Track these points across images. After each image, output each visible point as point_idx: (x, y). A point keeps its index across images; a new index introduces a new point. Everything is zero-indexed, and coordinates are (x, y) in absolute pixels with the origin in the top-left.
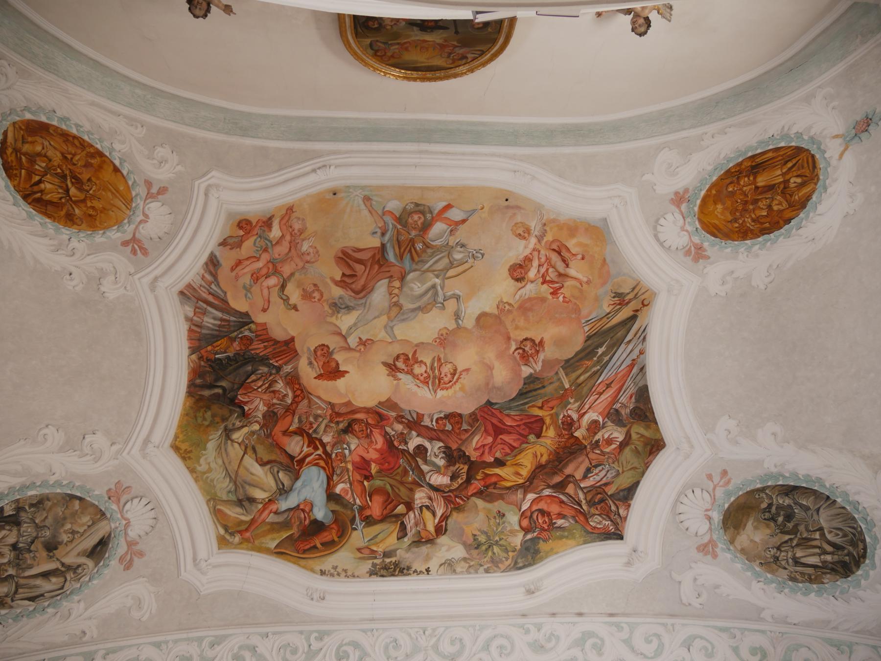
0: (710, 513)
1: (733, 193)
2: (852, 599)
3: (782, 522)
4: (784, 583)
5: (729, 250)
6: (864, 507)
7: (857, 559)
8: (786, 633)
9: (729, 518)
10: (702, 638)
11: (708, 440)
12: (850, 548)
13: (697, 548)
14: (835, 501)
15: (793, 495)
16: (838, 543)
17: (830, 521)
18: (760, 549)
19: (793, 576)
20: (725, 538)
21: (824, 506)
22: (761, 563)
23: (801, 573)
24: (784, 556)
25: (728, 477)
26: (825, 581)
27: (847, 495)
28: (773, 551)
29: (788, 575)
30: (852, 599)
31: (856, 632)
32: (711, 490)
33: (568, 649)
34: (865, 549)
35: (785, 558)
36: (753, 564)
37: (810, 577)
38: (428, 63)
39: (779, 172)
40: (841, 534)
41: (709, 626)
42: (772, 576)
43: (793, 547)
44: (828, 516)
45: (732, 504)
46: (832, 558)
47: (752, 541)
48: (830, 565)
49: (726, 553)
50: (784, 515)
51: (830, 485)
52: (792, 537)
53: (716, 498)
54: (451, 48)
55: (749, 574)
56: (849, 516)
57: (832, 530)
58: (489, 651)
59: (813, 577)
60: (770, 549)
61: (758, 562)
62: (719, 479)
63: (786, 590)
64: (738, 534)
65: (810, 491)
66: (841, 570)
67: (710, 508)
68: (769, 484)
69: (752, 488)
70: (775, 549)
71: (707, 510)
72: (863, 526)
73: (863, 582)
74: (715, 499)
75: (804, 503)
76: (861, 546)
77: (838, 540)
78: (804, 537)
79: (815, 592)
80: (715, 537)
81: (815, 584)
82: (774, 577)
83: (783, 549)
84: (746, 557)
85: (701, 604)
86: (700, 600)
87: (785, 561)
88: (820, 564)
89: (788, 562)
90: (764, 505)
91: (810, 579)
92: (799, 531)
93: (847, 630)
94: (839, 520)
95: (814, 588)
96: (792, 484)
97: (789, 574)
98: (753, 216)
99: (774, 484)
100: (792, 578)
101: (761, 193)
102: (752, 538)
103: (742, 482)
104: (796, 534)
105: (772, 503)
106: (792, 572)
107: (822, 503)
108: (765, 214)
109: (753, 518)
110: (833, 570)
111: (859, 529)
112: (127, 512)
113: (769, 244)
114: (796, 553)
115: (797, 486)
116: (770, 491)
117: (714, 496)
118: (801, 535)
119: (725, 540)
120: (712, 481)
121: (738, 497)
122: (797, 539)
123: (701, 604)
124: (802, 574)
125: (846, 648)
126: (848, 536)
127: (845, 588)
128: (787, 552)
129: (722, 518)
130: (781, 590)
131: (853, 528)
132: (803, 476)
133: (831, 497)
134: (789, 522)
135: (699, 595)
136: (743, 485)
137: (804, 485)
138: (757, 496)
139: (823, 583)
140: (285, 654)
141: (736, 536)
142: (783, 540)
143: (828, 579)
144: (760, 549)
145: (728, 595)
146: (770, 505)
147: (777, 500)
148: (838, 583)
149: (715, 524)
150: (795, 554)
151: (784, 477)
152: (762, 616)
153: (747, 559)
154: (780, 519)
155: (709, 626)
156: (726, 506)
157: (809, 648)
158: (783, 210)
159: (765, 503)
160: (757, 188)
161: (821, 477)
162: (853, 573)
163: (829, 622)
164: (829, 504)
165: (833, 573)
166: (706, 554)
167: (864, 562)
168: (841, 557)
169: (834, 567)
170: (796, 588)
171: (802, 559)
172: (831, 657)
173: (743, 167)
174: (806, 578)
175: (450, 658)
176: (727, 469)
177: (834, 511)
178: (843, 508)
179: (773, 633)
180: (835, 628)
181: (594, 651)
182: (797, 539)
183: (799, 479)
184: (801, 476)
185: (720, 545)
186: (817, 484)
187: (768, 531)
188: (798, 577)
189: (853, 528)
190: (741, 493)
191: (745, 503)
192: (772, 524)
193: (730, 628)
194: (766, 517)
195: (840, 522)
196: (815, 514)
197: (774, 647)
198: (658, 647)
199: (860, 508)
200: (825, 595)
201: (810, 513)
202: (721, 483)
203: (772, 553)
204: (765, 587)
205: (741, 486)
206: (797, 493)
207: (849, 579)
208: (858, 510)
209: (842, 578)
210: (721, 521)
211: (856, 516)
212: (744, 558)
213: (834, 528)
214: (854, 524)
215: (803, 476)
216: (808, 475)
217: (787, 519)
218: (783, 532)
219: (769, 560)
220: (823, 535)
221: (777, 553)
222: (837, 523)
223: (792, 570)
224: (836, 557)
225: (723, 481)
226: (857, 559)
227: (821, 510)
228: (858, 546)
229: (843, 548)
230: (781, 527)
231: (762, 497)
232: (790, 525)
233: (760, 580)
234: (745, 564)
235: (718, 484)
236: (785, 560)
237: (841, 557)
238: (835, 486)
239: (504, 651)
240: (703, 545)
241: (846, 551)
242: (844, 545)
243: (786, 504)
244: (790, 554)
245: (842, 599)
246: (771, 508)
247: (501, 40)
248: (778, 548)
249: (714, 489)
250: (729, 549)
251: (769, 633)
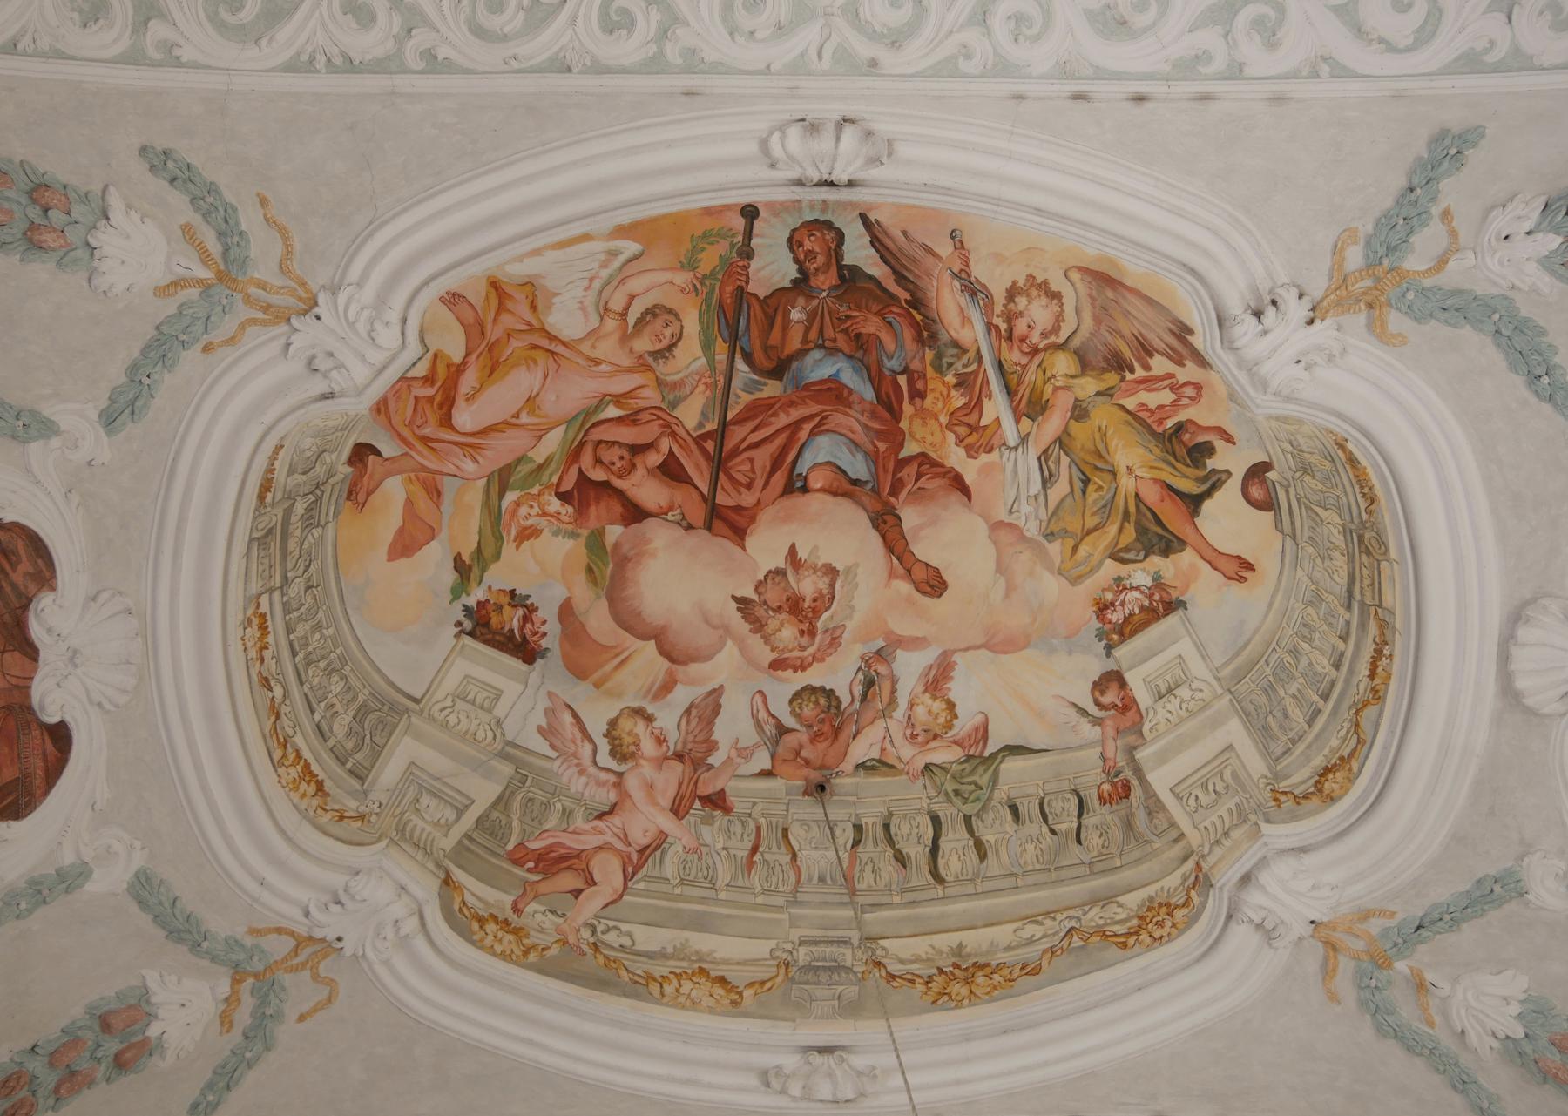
33: (1190, 31)
58: (987, 28)
112: (42, 610)
140: (473, 11)
175: (888, 41)
181: (1257, 38)
198: (1425, 22)
239: (1024, 29)
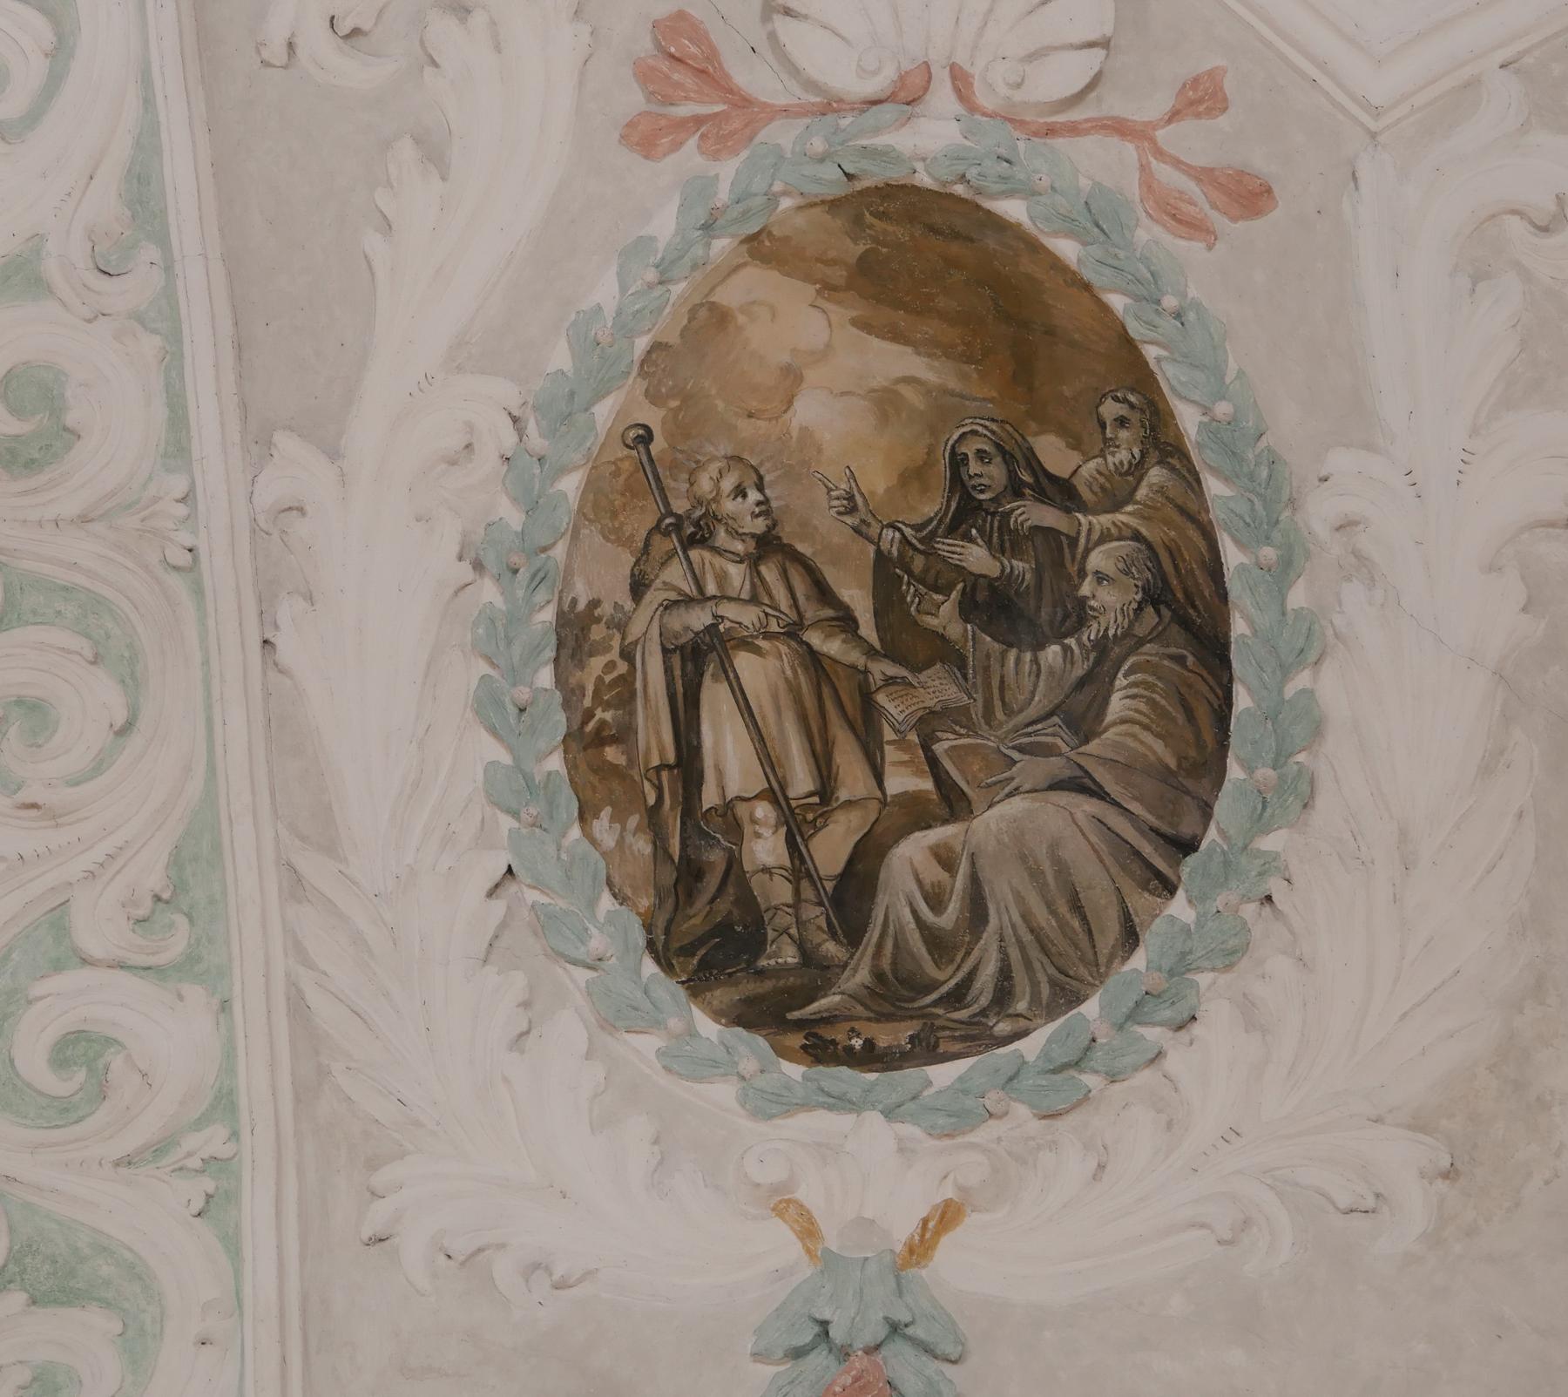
0: (942, 97)
2: (519, 980)
3: (960, 569)
4: (539, 579)
6: (1160, 1054)
7: (795, 1015)
8: (198, 591)
9: (933, 229)
10: (61, 53)
11: (1473, 84)
12: (861, 976)
13: (681, 15)
14: (1169, 888)
15: (1156, 636)
16: (882, 900)
17: (1023, 858)
18: (746, 428)
19: (597, 632)
20: (786, 203)
22: (646, 437)
23: (626, 681)
24: (722, 578)
25: (1218, 220)
26: (603, 826)
27: (1230, 956)
28: (742, 511)
29: (594, 604)
30: (519, 980)
31: (298, 1006)
32: (1112, 104)
35: (711, 589)
36: (635, 385)
37: (615, 740)
41: (148, 102)
42: (573, 501)
43: (793, 632)
44: (1054, 846)
45: (1034, 247)
46: (766, 870)
47: (792, 378)
48: (715, 857)
49: (684, 208)
50: (1008, 578)
51: (1276, 856)
52: (868, 630)
53: (1059, 142)
55: (560, 358)
56: (1083, 971)
57: (963, 868)
59: (612, 754)
60: (754, 496)
61: (652, 417)
62: (1200, 161)
63: (489, 592)
64: (828, 289)
65: (1209, 737)
66: (696, 921)
67: (983, 99)
68: (1214, 487)
69: (1169, 374)
70: (760, 526)
71: (961, 81)
72: (1030, 1047)
73: (649, 1043)
74: (1051, 131)
75: (1117, 705)
76: (891, 1036)
78: (881, 698)
79: (518, 766)
80: (782, 135)
81: (571, 766)
82: (564, 521)
83: (769, 572)
84: (673, 339)
85: (291, 46)
86: (318, 44)
87: (688, 587)
88: (710, 797)
89: (687, 601)
90: (1054, 454)
91: (600, 739)
92: (917, 669)
93: (297, 949)
94: (1042, 916)
95: (542, 757)
96: (1239, 627)
97: (606, 609)
99: (1217, 514)
100: (585, 630)
102: (811, 375)
103: (1197, 306)
104: (890, 652)
105: (1084, 508)
106: (621, 626)
107: (1135, 807)
109: (953, 383)
110: (690, 873)
111: (1003, 1028)
114: (758, 651)
115: (1226, 662)
116: (1161, 490)
117: (1073, 129)
118: (890, 681)
119: (772, 199)
120: (1174, 116)
121: (1087, 287)
122: (856, 657)
123: (291, 46)
124: (624, 692)
125: (177, 945)
127: (583, 937)
128: (754, 600)
129: (924, 180)
130: (490, 560)
131: (1003, 995)
132: (1308, 693)
133: (1191, 860)
134: (967, 610)
135: (356, 32)
136: (1178, 315)
137: (1242, 699)
138: (1110, 409)
139: (585, 815)
141: (808, 278)
142: (831, 575)
143: (621, 842)
144: (746, 428)
145: (387, 226)
146: (1062, 492)
147: (1105, 538)
148: (607, 902)
149: (877, 131)
150: (746, 644)
151: (1283, 573)
152: (286, 443)
153: (657, 347)
154: (977, 557)
155: (148, 102)
156: (1013, 210)
157: (125, 730)
159: (1075, 458)
161: (1321, 802)
162: (696, 986)
163: (330, 848)
164: (1137, 854)
165: (668, 876)
166: (645, 75)
167: (782, 1052)
169: (712, 882)
170: (517, 650)
171: (723, 690)
172: (98, 854)
174: (599, 714)
176: (1276, 215)
178: (1131, 937)
179: (182, 510)
180: (296, 886)
182: (856, 657)
183: (1286, 671)
184: (1302, 680)
185: (727, 171)
186: (1265, 773)
187: (876, 481)
188: (597, 664)
189: (1003, 995)
190: (1117, 302)
191: (1050, 332)
192: (930, 506)
193: (163, 241)
194: (974, 467)
195: (1026, 916)
196: (1054, 767)
197: (84, 519)
199: (1153, 1034)
200: (506, 823)
201: (1055, 734)
202: (1165, 174)
203: (729, 506)
204: (487, 462)
205: (1170, 302)
206: (1180, 660)
207: (650, 967)
208: (1136, 1014)
209: (648, 928)
210: (895, 175)
211: (1091, 1008)
212: (668, 326)
213: (975, 880)
214: (1035, 999)
215: (1308, 693)
216: (1317, 730)
217: (981, 596)
218: (886, 576)
219: (677, 487)
220: (915, 814)
221: (735, 534)
222: (1019, 899)
223: (636, 630)
224: (782, 891)
225: (1192, 188)
226: (795, 1015)
227: (1087, 806)
229: (851, 928)
230: (918, 563)
231: (1109, 444)
232: (945, 617)
233: (532, 428)
234: (625, 327)
235: (1159, 153)
236: (700, 589)
237: (785, 919)
238: (1275, 886)
240: (713, 55)
241: (831, 948)
242: (873, 935)
243: (1086, 589)
244: (749, 616)
245: (504, 925)
246: (1042, 496)
248: (768, 545)
249: (1120, 128)
250: (708, 228)
251: (179, 485)
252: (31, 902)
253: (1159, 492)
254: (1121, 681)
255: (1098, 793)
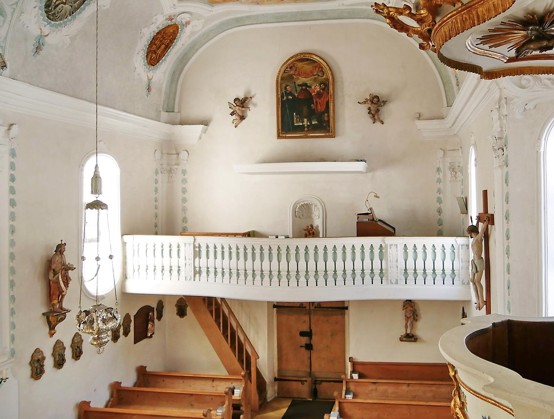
1: (169, 37)
5: (160, 27)
16: (57, 8)
21: (71, 10)
34: (50, 19)
38: (303, 64)
39: (159, 53)
40: (59, 11)
54: (296, 74)
72: (57, 23)
75: (77, 3)
76: (52, 17)
77: (58, 9)
98: (159, 38)
101: (161, 44)
108: (156, 42)
113: (149, 39)
126: (57, 14)
158: (151, 48)
160: (163, 44)
168: (52, 6)
173: (171, 44)
177: (68, 12)
227: (71, 8)
228: (52, 16)
241: (53, 9)
247: (279, 80)
252: (13, 154)
253: (440, 183)
254: (79, 1)
255: (72, 7)
